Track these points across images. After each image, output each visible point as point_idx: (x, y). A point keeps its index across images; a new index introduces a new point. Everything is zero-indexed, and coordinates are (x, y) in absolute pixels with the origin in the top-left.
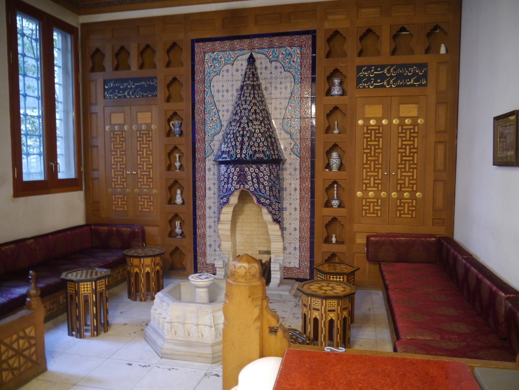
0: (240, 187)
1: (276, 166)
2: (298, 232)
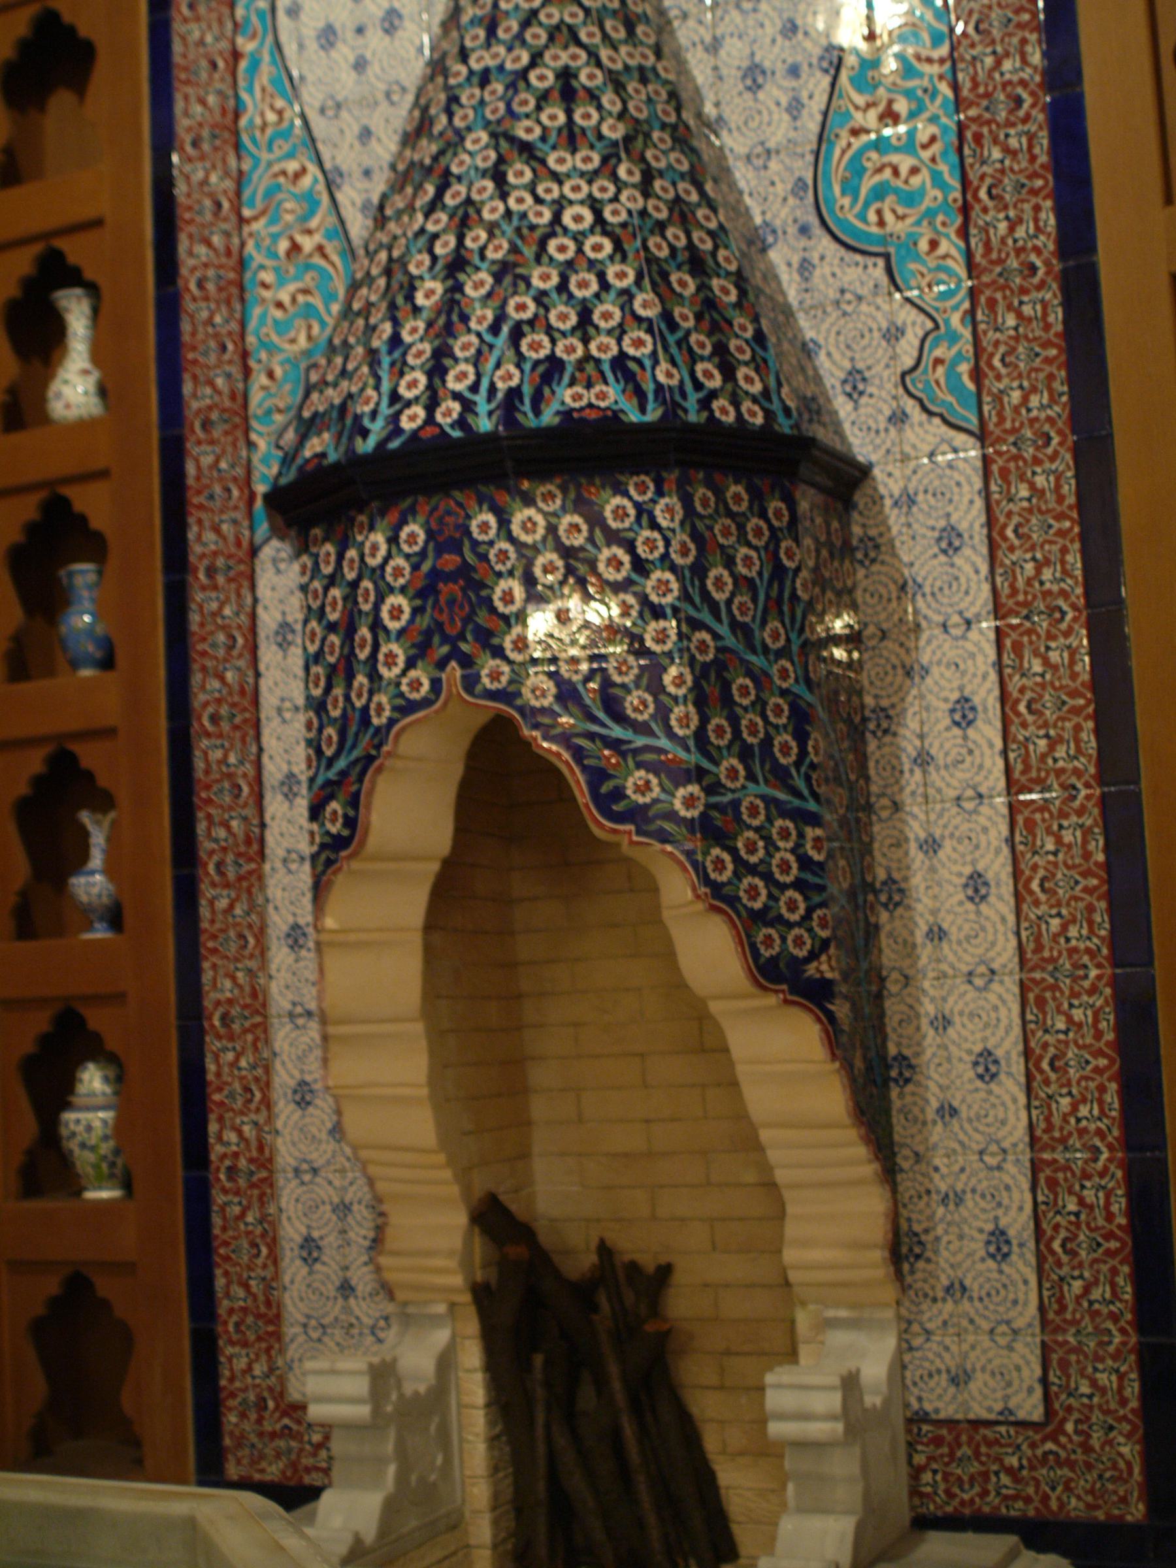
0: (436, 684)
1: (757, 496)
2: (1010, 1086)
